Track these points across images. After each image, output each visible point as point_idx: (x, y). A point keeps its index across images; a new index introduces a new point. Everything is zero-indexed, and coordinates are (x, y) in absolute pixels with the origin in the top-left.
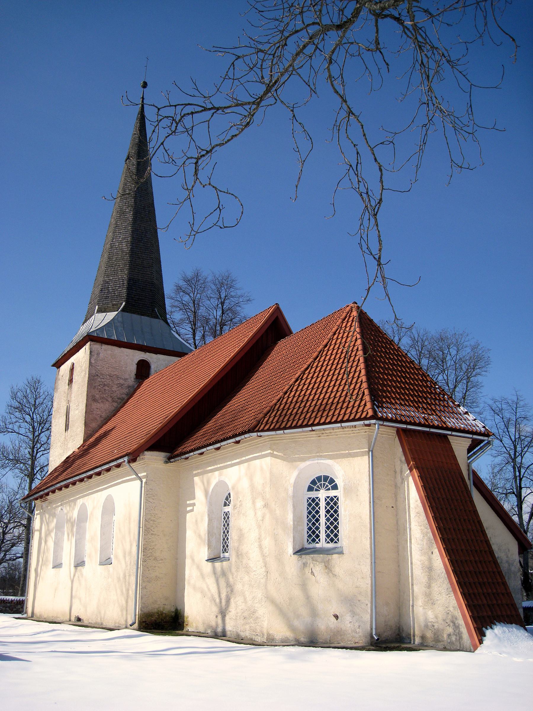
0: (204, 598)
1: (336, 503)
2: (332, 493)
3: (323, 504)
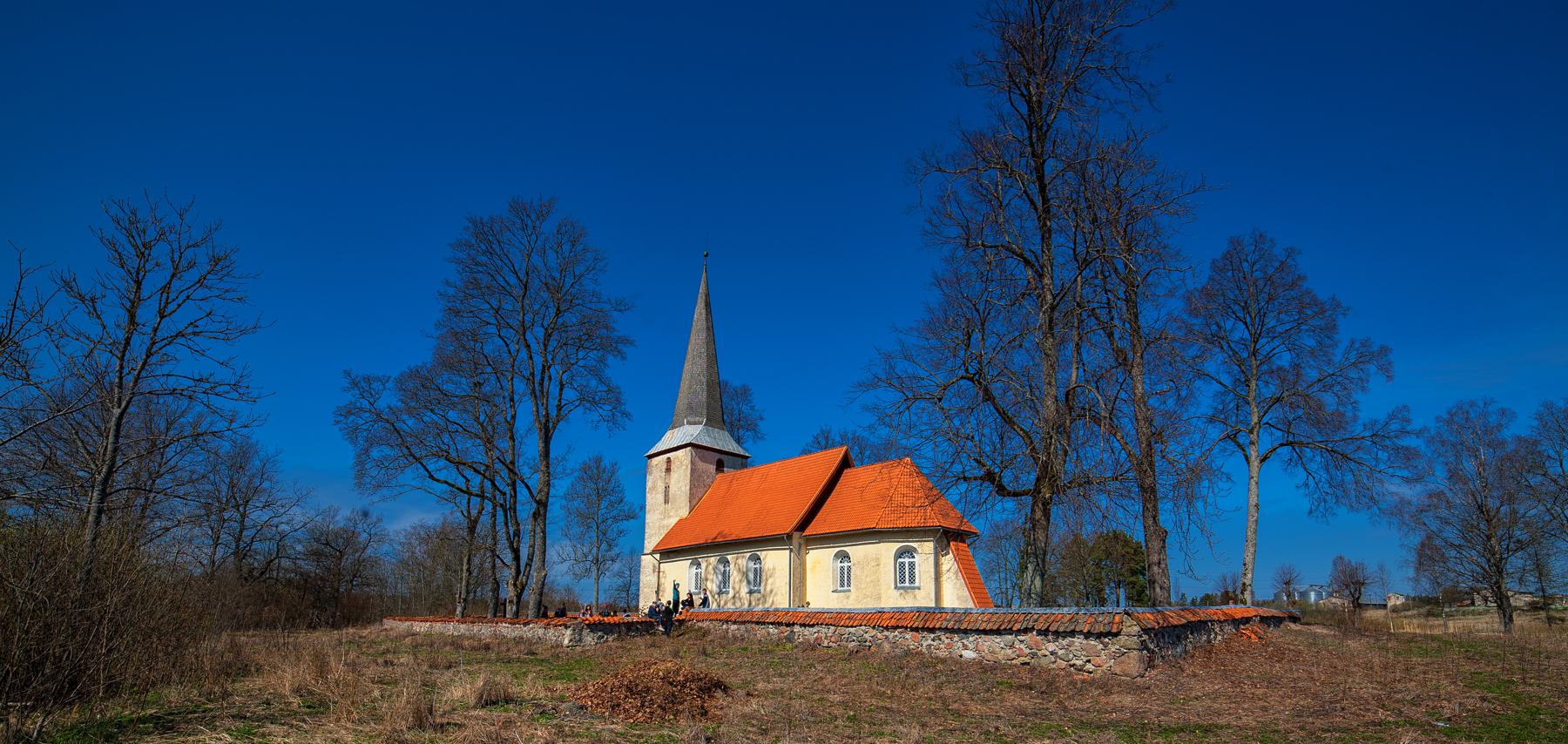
2: (912, 560)
3: (907, 565)
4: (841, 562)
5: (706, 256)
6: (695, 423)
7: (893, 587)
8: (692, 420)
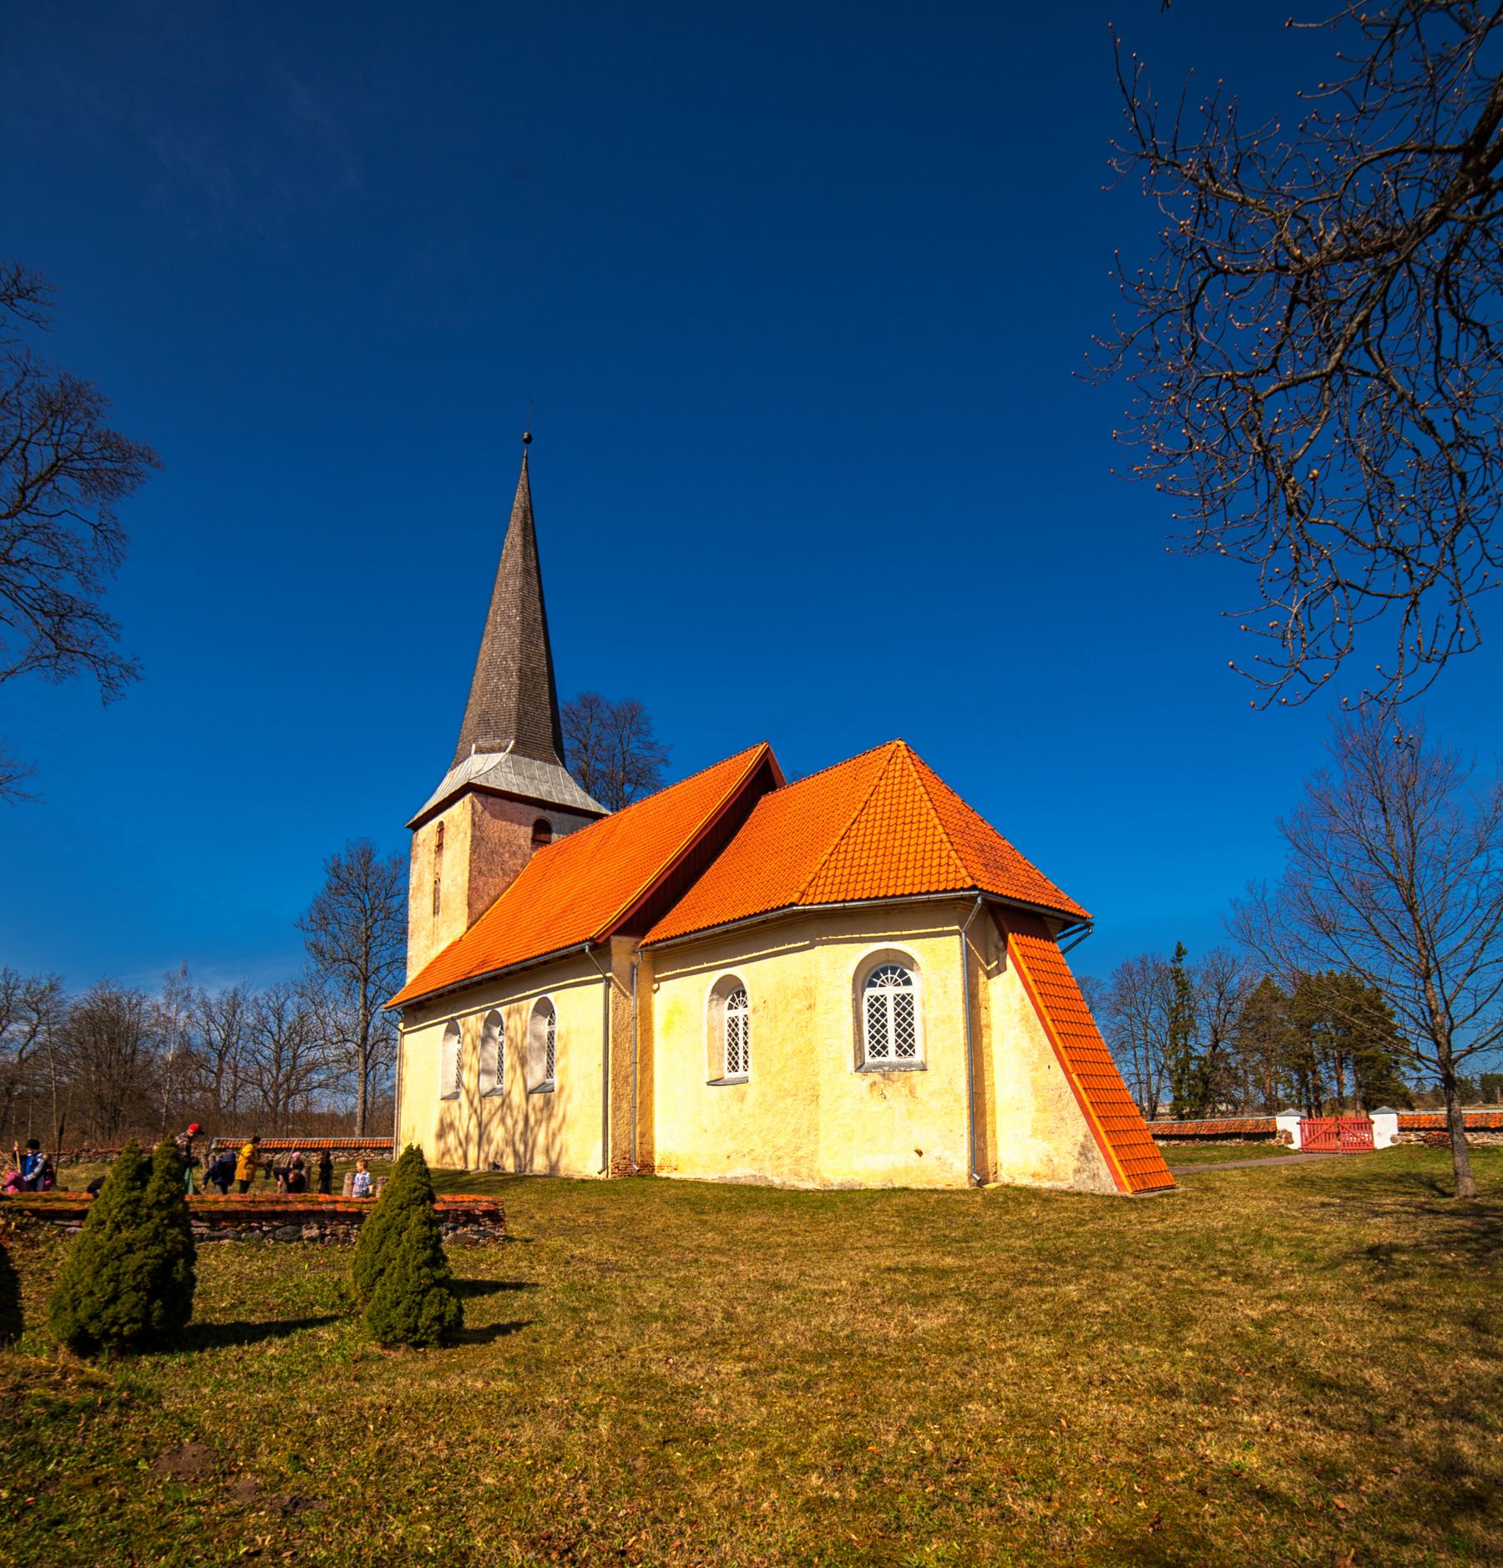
0: (515, 1228)
1: (909, 1003)
2: (903, 990)
3: (890, 1005)
4: (730, 1007)
5: (528, 440)
6: (491, 750)
7: (850, 1064)
8: (487, 745)
